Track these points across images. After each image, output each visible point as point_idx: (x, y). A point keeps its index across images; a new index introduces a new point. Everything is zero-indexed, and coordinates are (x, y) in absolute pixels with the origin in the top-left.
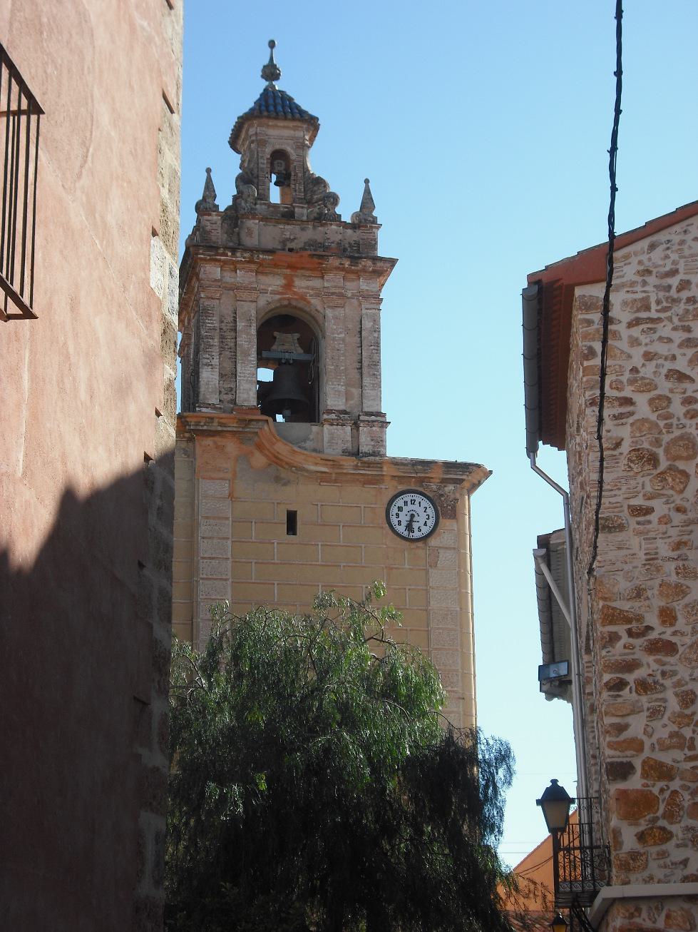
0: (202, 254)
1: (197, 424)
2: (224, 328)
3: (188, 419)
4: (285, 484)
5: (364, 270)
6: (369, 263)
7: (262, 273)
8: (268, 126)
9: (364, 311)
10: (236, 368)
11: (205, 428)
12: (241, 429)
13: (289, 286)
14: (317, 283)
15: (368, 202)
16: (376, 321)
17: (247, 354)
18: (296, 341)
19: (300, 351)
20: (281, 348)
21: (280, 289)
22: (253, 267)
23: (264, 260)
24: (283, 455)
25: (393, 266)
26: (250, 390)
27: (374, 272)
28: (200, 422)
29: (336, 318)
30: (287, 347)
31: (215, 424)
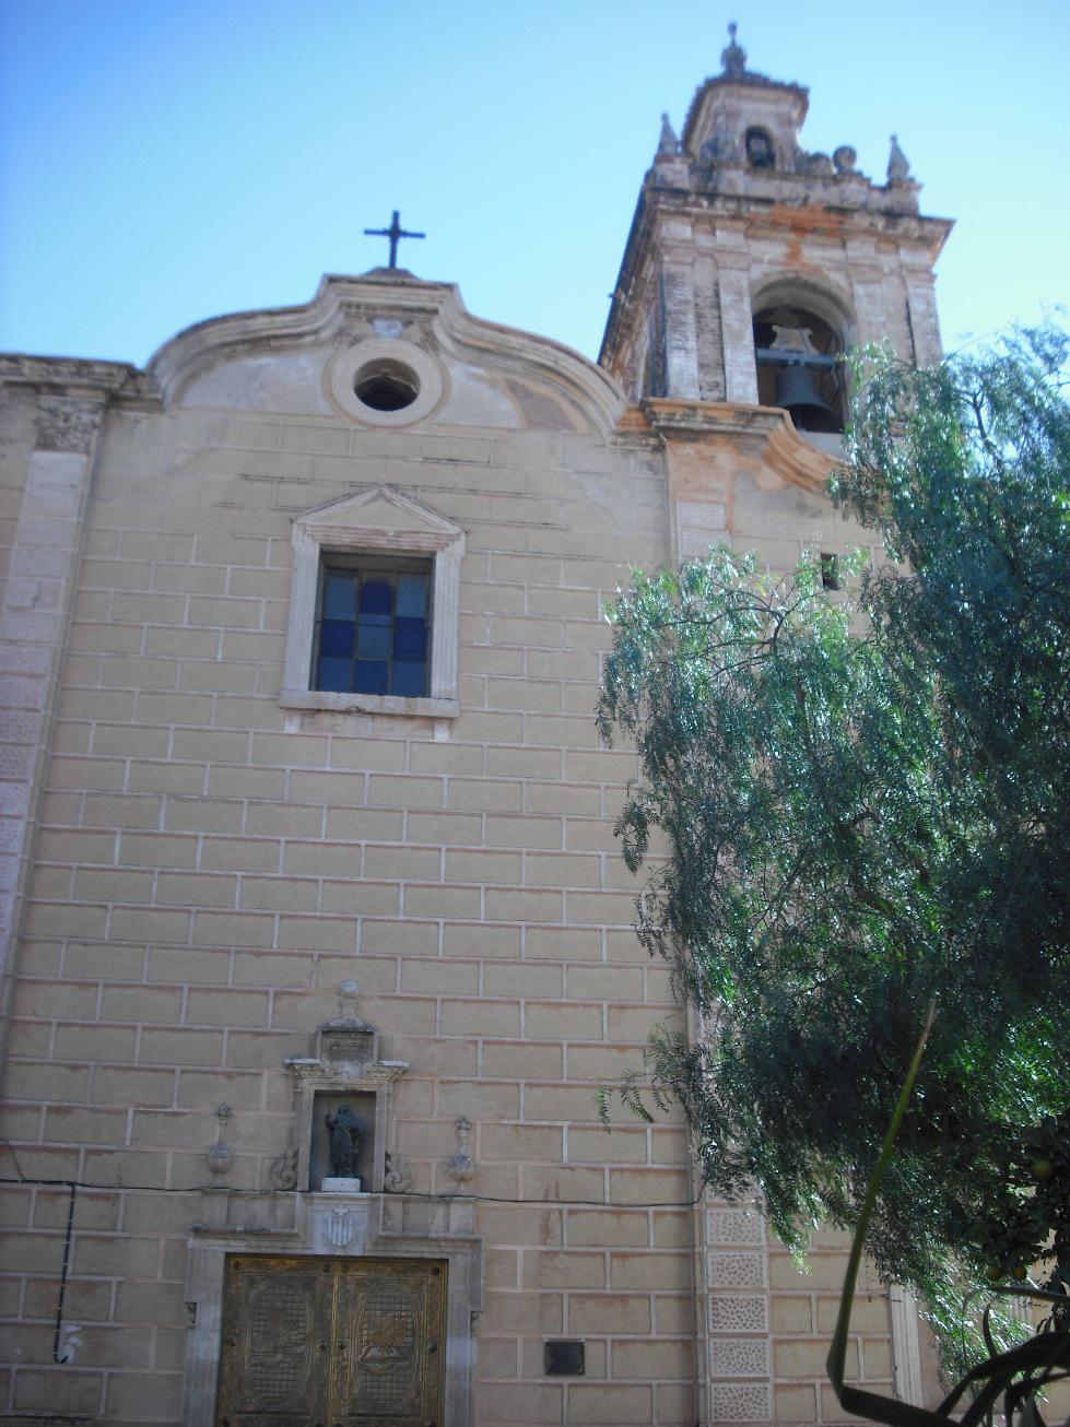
0: (664, 203)
1: (671, 417)
2: (702, 305)
3: (656, 409)
4: (815, 515)
5: (906, 236)
6: (913, 224)
7: (753, 237)
8: (740, 97)
9: (911, 290)
10: (722, 356)
11: (683, 425)
12: (739, 429)
13: (794, 254)
14: (837, 254)
15: (897, 163)
16: (930, 303)
17: (738, 337)
18: (807, 339)
19: (814, 351)
20: (784, 347)
21: (782, 259)
22: (741, 225)
23: (755, 217)
24: (808, 468)
25: (947, 233)
26: (748, 384)
27: (921, 239)
28: (674, 415)
29: (870, 296)
30: (792, 346)
31: (699, 418)
